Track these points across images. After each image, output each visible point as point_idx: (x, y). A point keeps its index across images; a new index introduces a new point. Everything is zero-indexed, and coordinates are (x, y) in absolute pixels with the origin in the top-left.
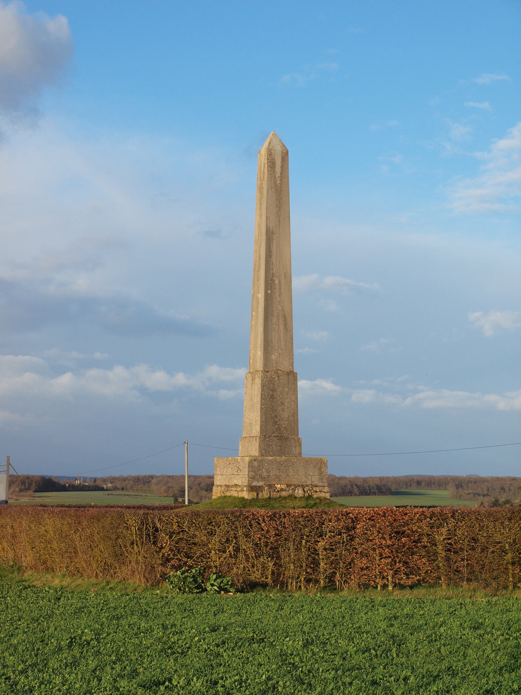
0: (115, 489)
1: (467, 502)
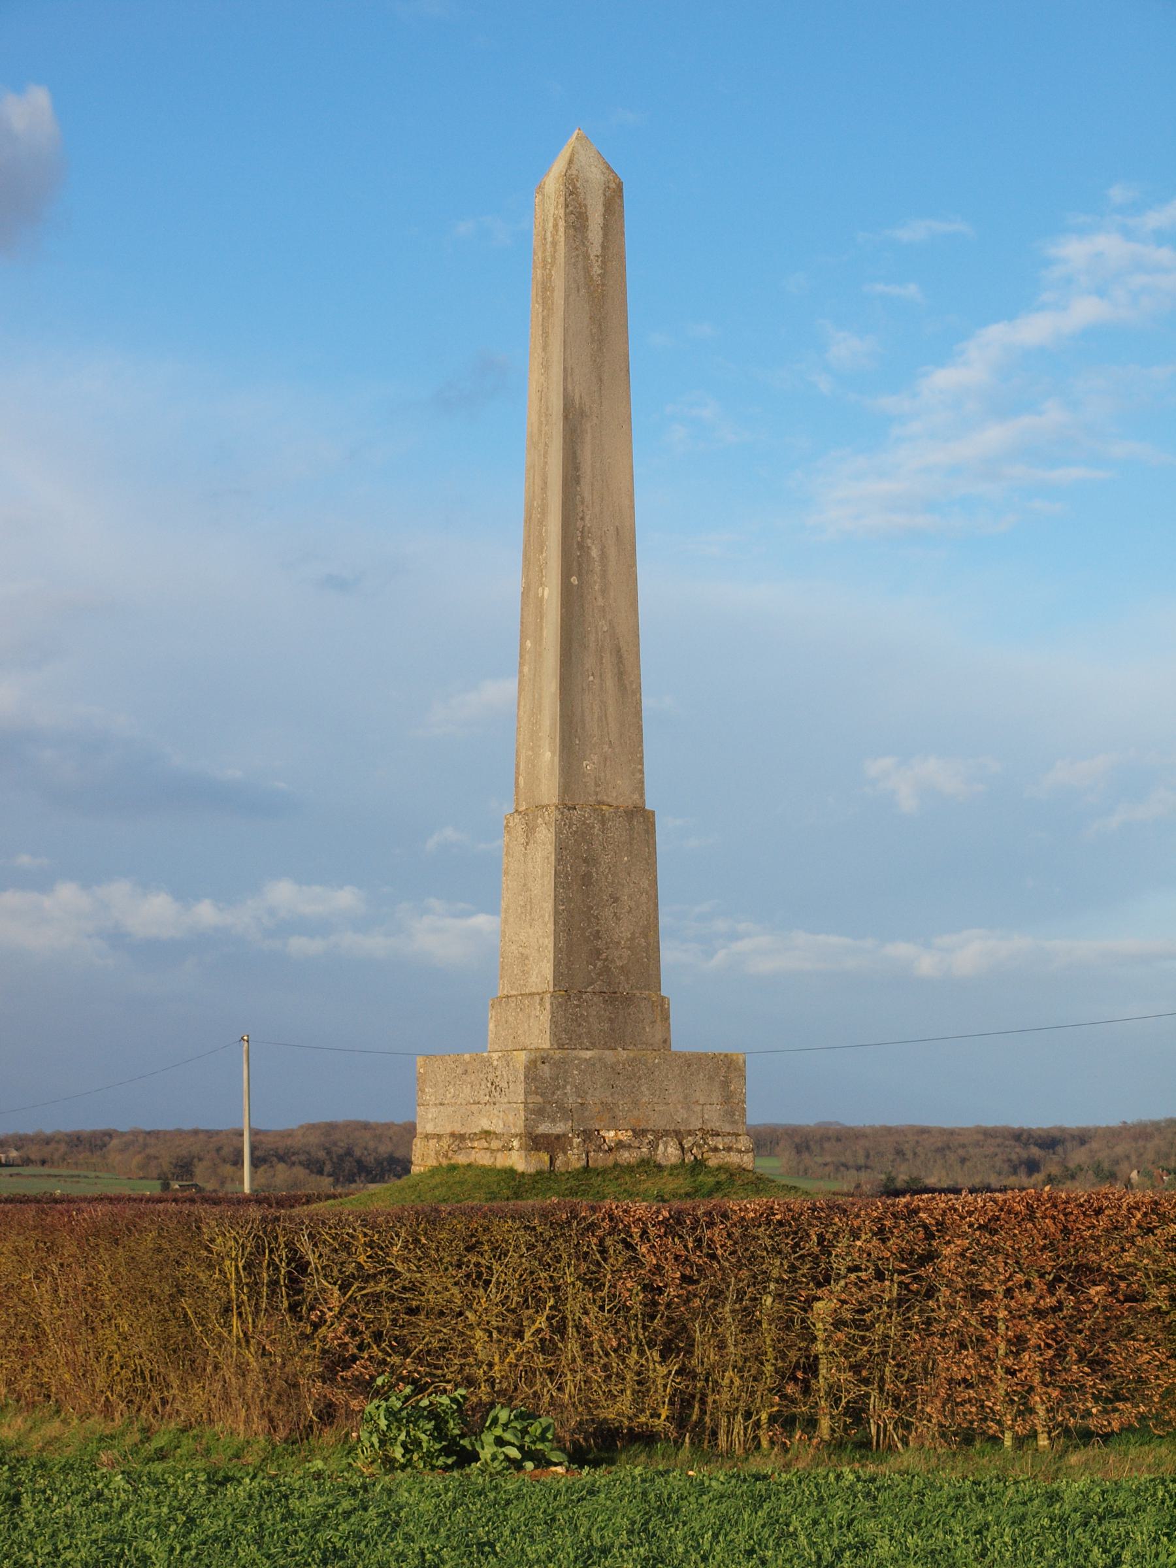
0: (27, 1162)
1: (822, 1183)
